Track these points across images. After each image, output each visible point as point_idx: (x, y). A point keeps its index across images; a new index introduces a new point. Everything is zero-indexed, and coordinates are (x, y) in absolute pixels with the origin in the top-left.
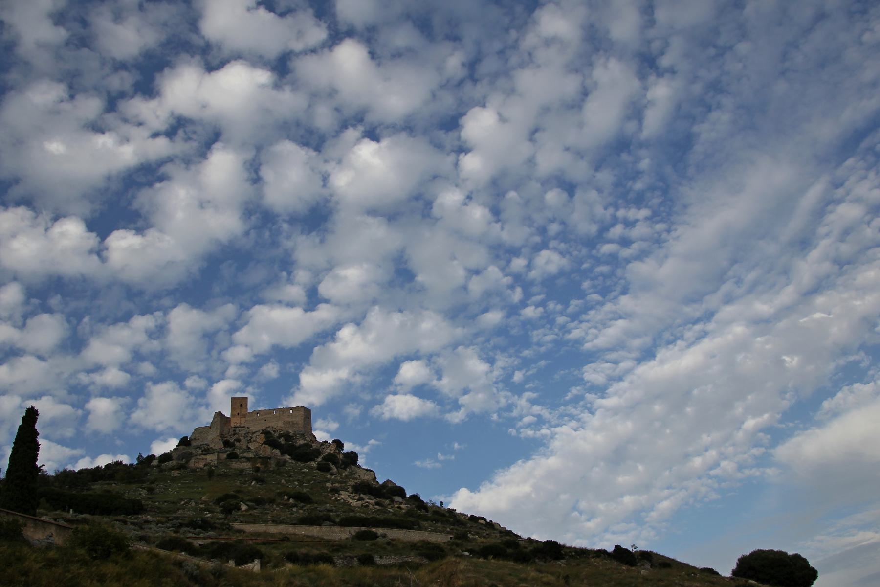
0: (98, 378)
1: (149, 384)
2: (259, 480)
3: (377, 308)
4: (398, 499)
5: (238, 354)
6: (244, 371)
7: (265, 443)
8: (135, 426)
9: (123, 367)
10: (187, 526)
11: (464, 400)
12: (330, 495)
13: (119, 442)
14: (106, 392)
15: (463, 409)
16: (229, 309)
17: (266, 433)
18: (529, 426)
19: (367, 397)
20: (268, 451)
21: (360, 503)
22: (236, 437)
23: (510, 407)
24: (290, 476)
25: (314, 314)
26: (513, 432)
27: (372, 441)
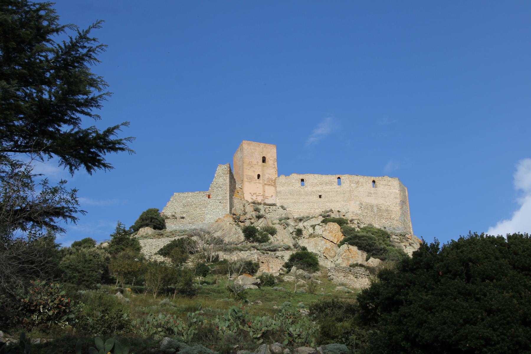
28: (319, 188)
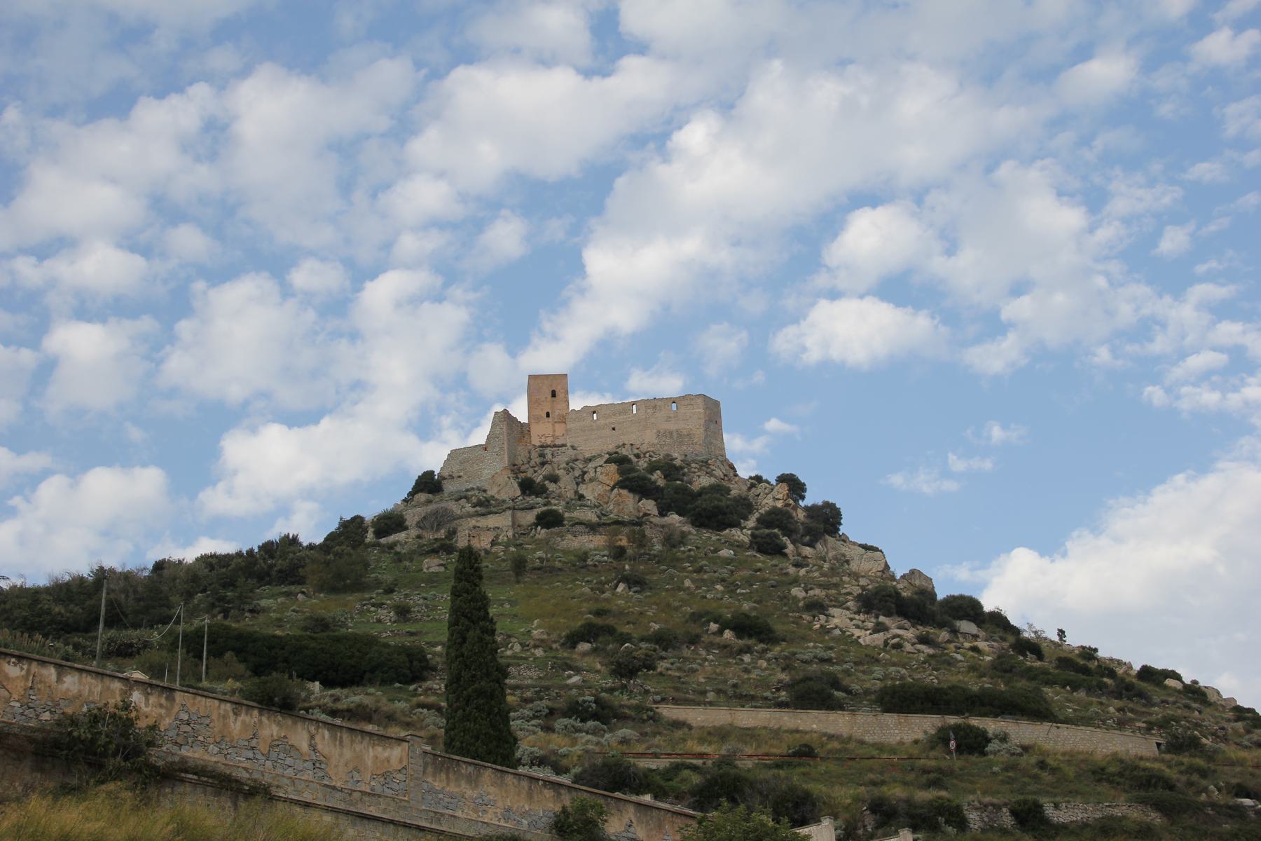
0: (65, 270)
1: (200, 285)
2: (635, 582)
3: (777, 65)
4: (967, 626)
5: (423, 196)
6: (434, 242)
7: (620, 485)
8: (172, 393)
9: (131, 242)
10: (566, 714)
11: (1019, 309)
12: (807, 617)
13: (136, 434)
14: (87, 308)
15: (1012, 337)
16: (391, 75)
17: (619, 460)
18: (1204, 377)
19: (755, 304)
20: (628, 505)
21: (880, 638)
22: (547, 470)
23: (1145, 329)
24: (699, 570)
25: (611, 82)
26: (1155, 394)
27: (773, 424)
28: (611, 420)
